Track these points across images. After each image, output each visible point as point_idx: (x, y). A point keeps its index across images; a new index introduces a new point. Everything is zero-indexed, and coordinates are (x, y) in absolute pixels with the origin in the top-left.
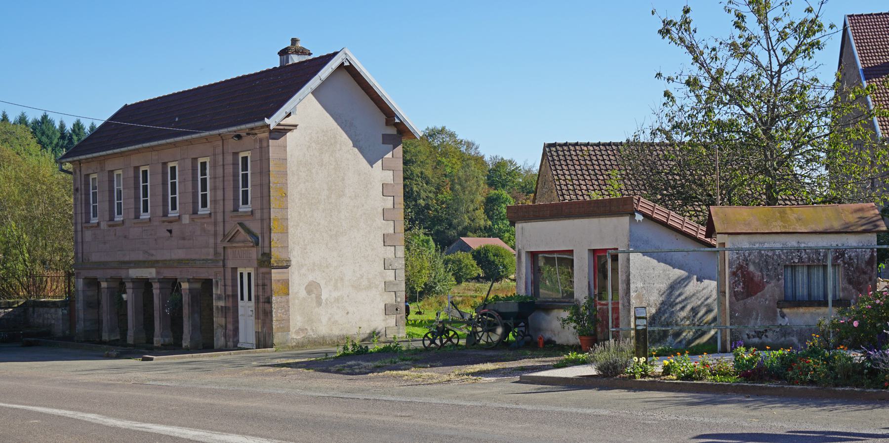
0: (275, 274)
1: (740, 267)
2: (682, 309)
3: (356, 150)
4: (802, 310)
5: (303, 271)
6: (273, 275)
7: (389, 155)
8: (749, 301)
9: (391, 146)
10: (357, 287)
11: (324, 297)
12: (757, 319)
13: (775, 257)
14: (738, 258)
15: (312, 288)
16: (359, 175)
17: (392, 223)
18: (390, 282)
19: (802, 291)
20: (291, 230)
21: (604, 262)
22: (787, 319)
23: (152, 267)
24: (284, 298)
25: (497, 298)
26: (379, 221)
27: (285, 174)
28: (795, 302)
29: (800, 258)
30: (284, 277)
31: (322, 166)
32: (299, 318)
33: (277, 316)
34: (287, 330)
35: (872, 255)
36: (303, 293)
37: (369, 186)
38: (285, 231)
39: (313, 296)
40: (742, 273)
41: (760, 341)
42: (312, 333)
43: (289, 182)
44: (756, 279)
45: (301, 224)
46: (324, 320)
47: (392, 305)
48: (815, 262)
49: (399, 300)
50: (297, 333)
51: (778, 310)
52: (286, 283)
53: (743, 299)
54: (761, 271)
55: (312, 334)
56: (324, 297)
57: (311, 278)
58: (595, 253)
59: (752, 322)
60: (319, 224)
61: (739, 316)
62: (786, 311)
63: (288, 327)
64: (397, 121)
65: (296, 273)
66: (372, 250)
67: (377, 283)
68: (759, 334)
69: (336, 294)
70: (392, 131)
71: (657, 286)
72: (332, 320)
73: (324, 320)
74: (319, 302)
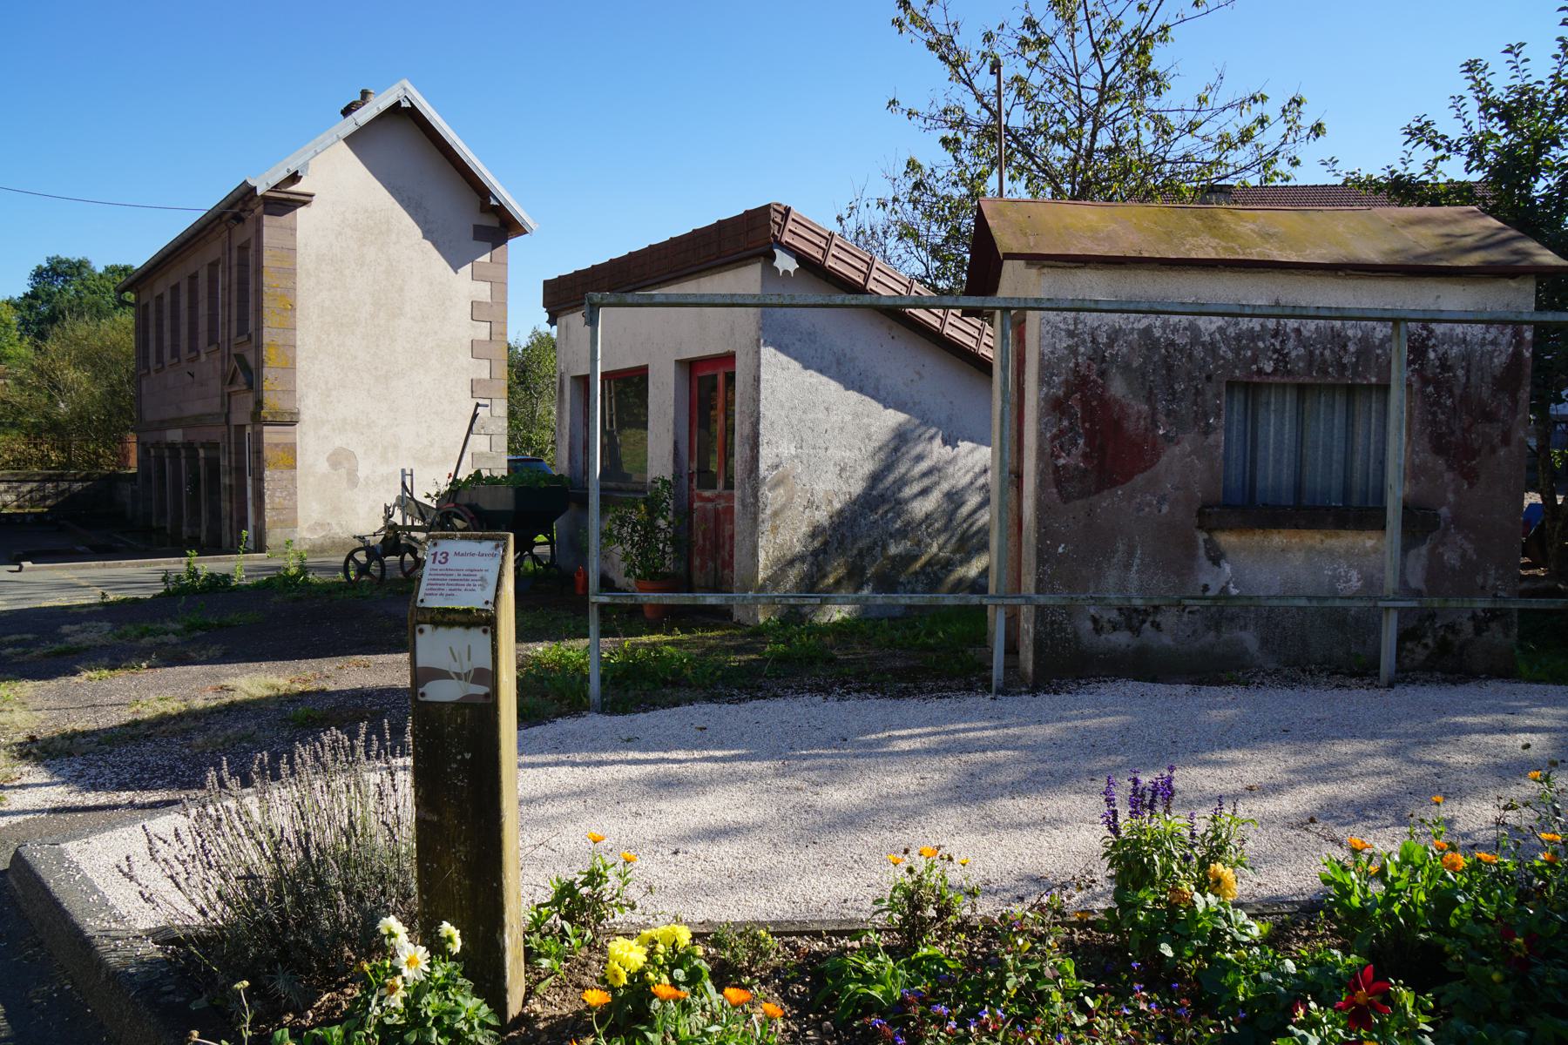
0: (270, 435)
1: (1079, 382)
2: (924, 492)
3: (428, 245)
4: (1278, 539)
6: (266, 436)
7: (486, 258)
8: (1106, 501)
12: (1128, 567)
13: (1199, 352)
14: (1073, 350)
15: (340, 459)
16: (431, 284)
17: (487, 363)
18: (482, 454)
19: (1274, 473)
21: (712, 386)
22: (1227, 568)
23: (178, 427)
24: (287, 474)
26: (465, 358)
28: (1248, 507)
29: (1283, 357)
34: (293, 523)
35: (1516, 356)
36: (323, 466)
38: (290, 367)
39: (343, 471)
40: (1085, 403)
41: (1136, 642)
42: (339, 530)
43: (298, 285)
44: (1129, 426)
48: (1335, 377)
50: (312, 529)
51: (1202, 536)
52: (291, 450)
53: (1083, 494)
54: (1150, 398)
56: (363, 471)
57: (338, 442)
58: (690, 367)
59: (1112, 577)
61: (1068, 547)
62: (1226, 539)
64: (493, 202)
68: (1132, 618)
70: (490, 221)
71: (837, 454)
74: (353, 480)
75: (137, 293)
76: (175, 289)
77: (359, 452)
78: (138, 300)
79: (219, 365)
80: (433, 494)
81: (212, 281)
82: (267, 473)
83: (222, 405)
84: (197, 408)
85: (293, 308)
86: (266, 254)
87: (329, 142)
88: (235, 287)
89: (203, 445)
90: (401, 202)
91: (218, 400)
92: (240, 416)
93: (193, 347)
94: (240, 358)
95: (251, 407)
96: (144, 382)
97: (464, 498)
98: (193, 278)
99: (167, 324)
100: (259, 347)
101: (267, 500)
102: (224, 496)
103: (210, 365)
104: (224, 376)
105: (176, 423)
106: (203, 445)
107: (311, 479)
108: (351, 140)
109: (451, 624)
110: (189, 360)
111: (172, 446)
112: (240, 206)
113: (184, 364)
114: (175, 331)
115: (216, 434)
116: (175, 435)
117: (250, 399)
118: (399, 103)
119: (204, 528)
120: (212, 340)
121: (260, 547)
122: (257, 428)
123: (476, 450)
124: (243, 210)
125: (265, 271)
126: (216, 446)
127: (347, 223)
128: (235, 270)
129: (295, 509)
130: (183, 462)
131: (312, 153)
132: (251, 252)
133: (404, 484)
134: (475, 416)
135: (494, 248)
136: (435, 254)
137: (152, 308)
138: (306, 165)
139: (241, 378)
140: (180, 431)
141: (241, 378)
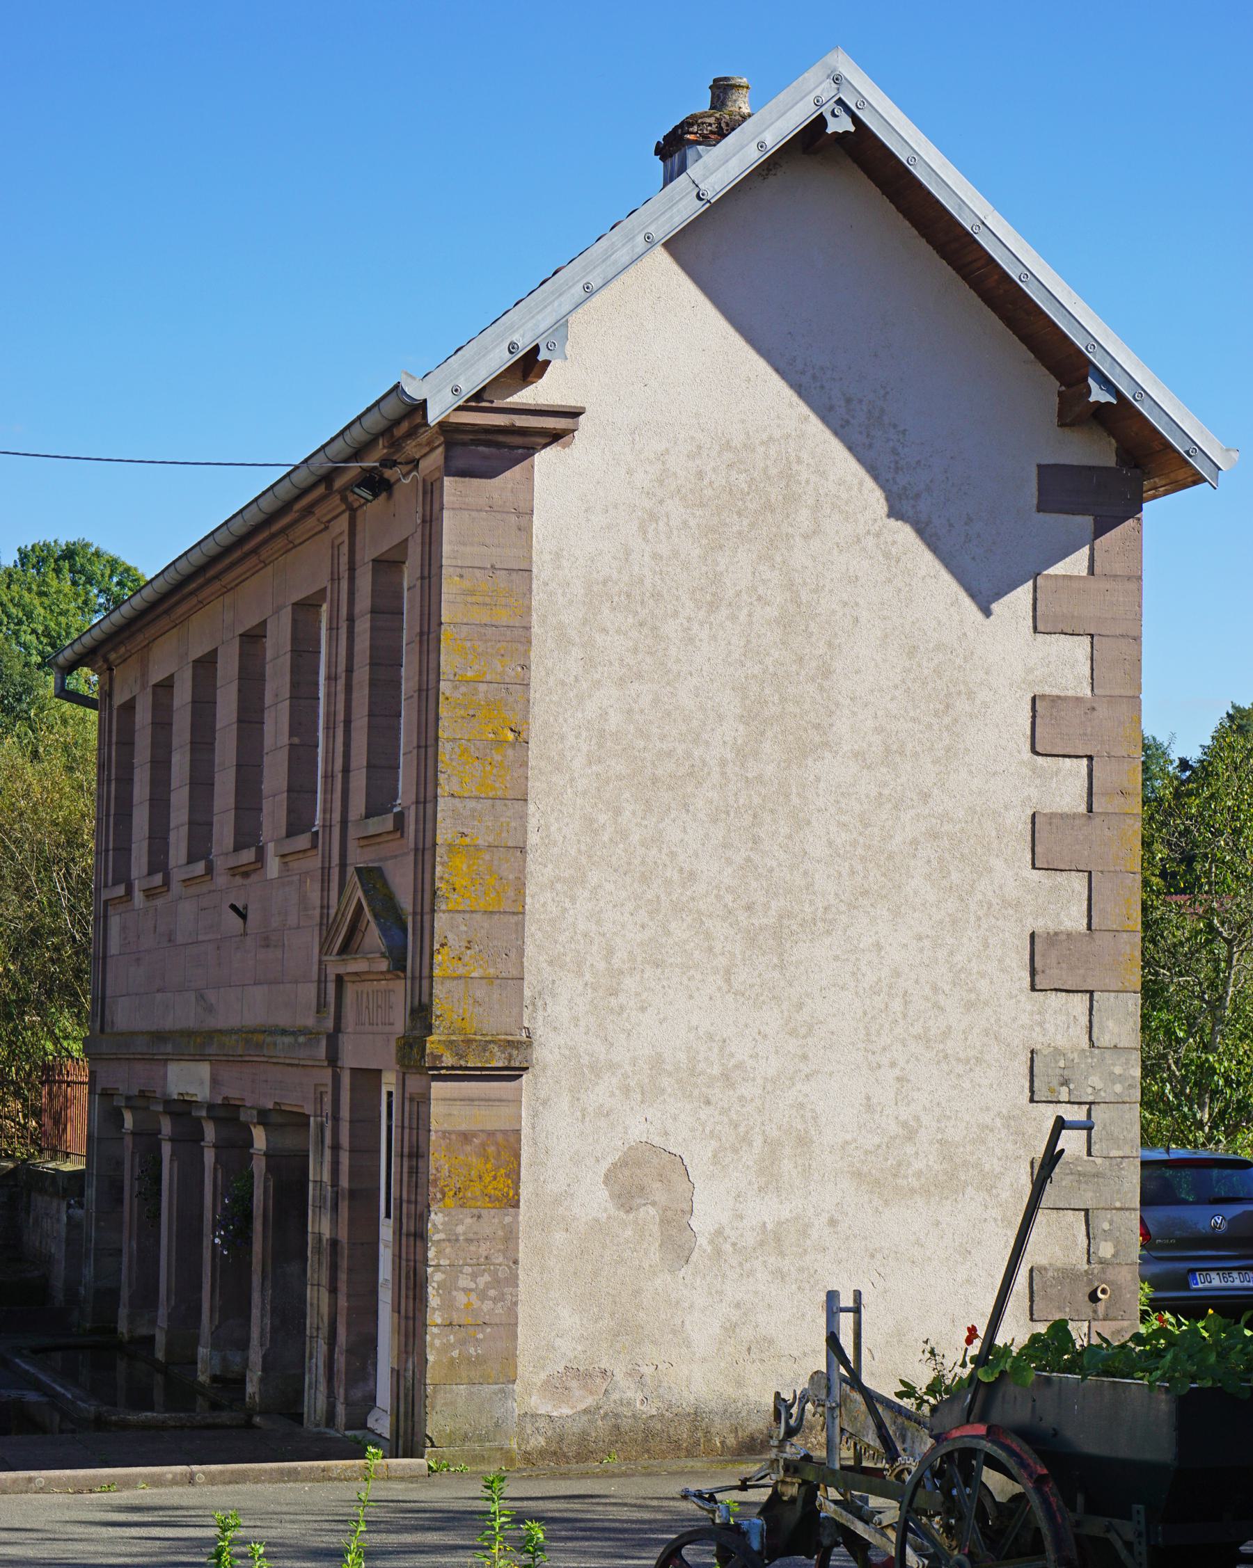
0: (450, 1108)
3: (904, 533)
5: (601, 1093)
6: (436, 1110)
7: (1075, 564)
9: (1087, 521)
10: (881, 1182)
11: (702, 1223)
15: (645, 1179)
16: (912, 652)
17: (1078, 883)
20: (538, 900)
23: (199, 1058)
24: (492, 1222)
25: (1052, 1344)
26: (1010, 870)
27: (519, 637)
30: (493, 1119)
31: (713, 607)
32: (568, 1318)
33: (448, 1305)
36: (593, 1200)
37: (962, 705)
38: (512, 911)
39: (649, 1213)
43: (536, 674)
45: (594, 877)
46: (703, 1330)
47: (1067, 1275)
49: (1106, 1250)
50: (555, 1388)
52: (505, 1150)
55: (632, 1399)
60: (692, 876)
63: (509, 1359)
64: (1098, 395)
65: (563, 1102)
66: (969, 1006)
67: (992, 1164)
69: (767, 1210)
70: (1094, 451)
72: (746, 1333)
73: (703, 1330)
74: (677, 1241)
75: (108, 671)
76: (206, 665)
77: (698, 1158)
78: (107, 692)
79: (315, 897)
80: (921, 1385)
81: (304, 651)
82: (436, 1218)
83: (321, 1006)
84: (247, 1008)
85: (521, 739)
86: (450, 588)
87: (623, 256)
88: (362, 674)
89: (264, 1117)
90: (825, 413)
91: (309, 992)
92: (370, 1046)
93: (247, 836)
94: (372, 878)
95: (399, 1022)
96: (115, 922)
97: (1014, 1408)
98: (253, 638)
99: (180, 762)
100: (425, 852)
101: (434, 1300)
102: (316, 1271)
103: (290, 890)
104: (327, 928)
105: (194, 1043)
106: (264, 1117)
107: (559, 1236)
108: (679, 246)
109: (1010, 322)
110: (233, 871)
111: (181, 1109)
112: (380, 451)
113: (221, 880)
114: (202, 784)
115: (299, 1090)
116: (189, 1080)
117: (399, 994)
118: (819, 122)
119: (256, 1356)
120: (297, 824)
121: (407, 1441)
122: (414, 1083)
123: (1042, 1261)
124: (388, 463)
125: (446, 633)
126: (300, 1121)
127: (678, 486)
128: (363, 626)
129: (510, 1327)
130: (209, 1157)
131: (578, 291)
132: (409, 575)
133: (833, 1340)
134: (1052, 1157)
135: (1100, 531)
136: (926, 560)
137: (143, 716)
138: (561, 325)
139: (373, 936)
140: (204, 1069)
141: (373, 936)
